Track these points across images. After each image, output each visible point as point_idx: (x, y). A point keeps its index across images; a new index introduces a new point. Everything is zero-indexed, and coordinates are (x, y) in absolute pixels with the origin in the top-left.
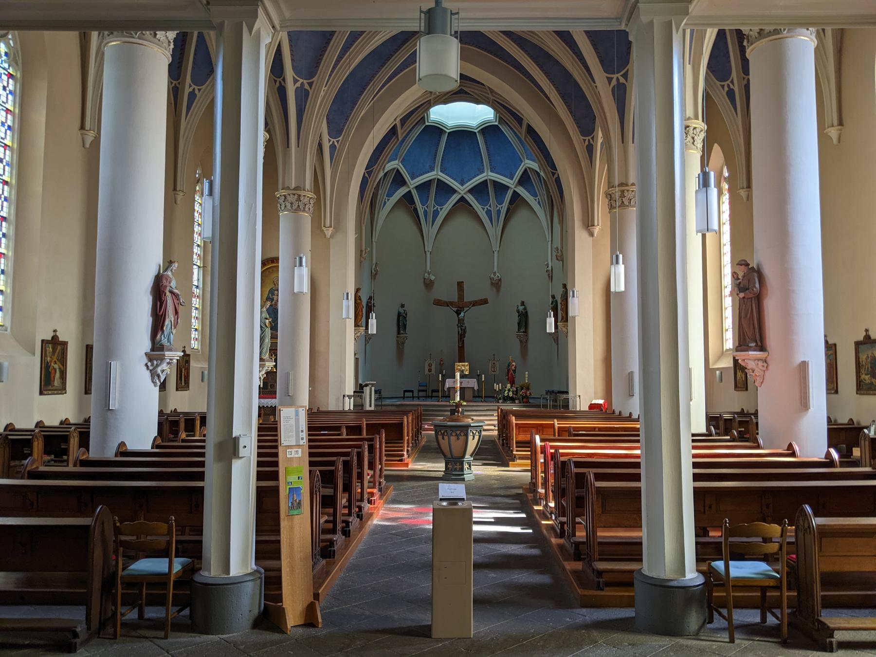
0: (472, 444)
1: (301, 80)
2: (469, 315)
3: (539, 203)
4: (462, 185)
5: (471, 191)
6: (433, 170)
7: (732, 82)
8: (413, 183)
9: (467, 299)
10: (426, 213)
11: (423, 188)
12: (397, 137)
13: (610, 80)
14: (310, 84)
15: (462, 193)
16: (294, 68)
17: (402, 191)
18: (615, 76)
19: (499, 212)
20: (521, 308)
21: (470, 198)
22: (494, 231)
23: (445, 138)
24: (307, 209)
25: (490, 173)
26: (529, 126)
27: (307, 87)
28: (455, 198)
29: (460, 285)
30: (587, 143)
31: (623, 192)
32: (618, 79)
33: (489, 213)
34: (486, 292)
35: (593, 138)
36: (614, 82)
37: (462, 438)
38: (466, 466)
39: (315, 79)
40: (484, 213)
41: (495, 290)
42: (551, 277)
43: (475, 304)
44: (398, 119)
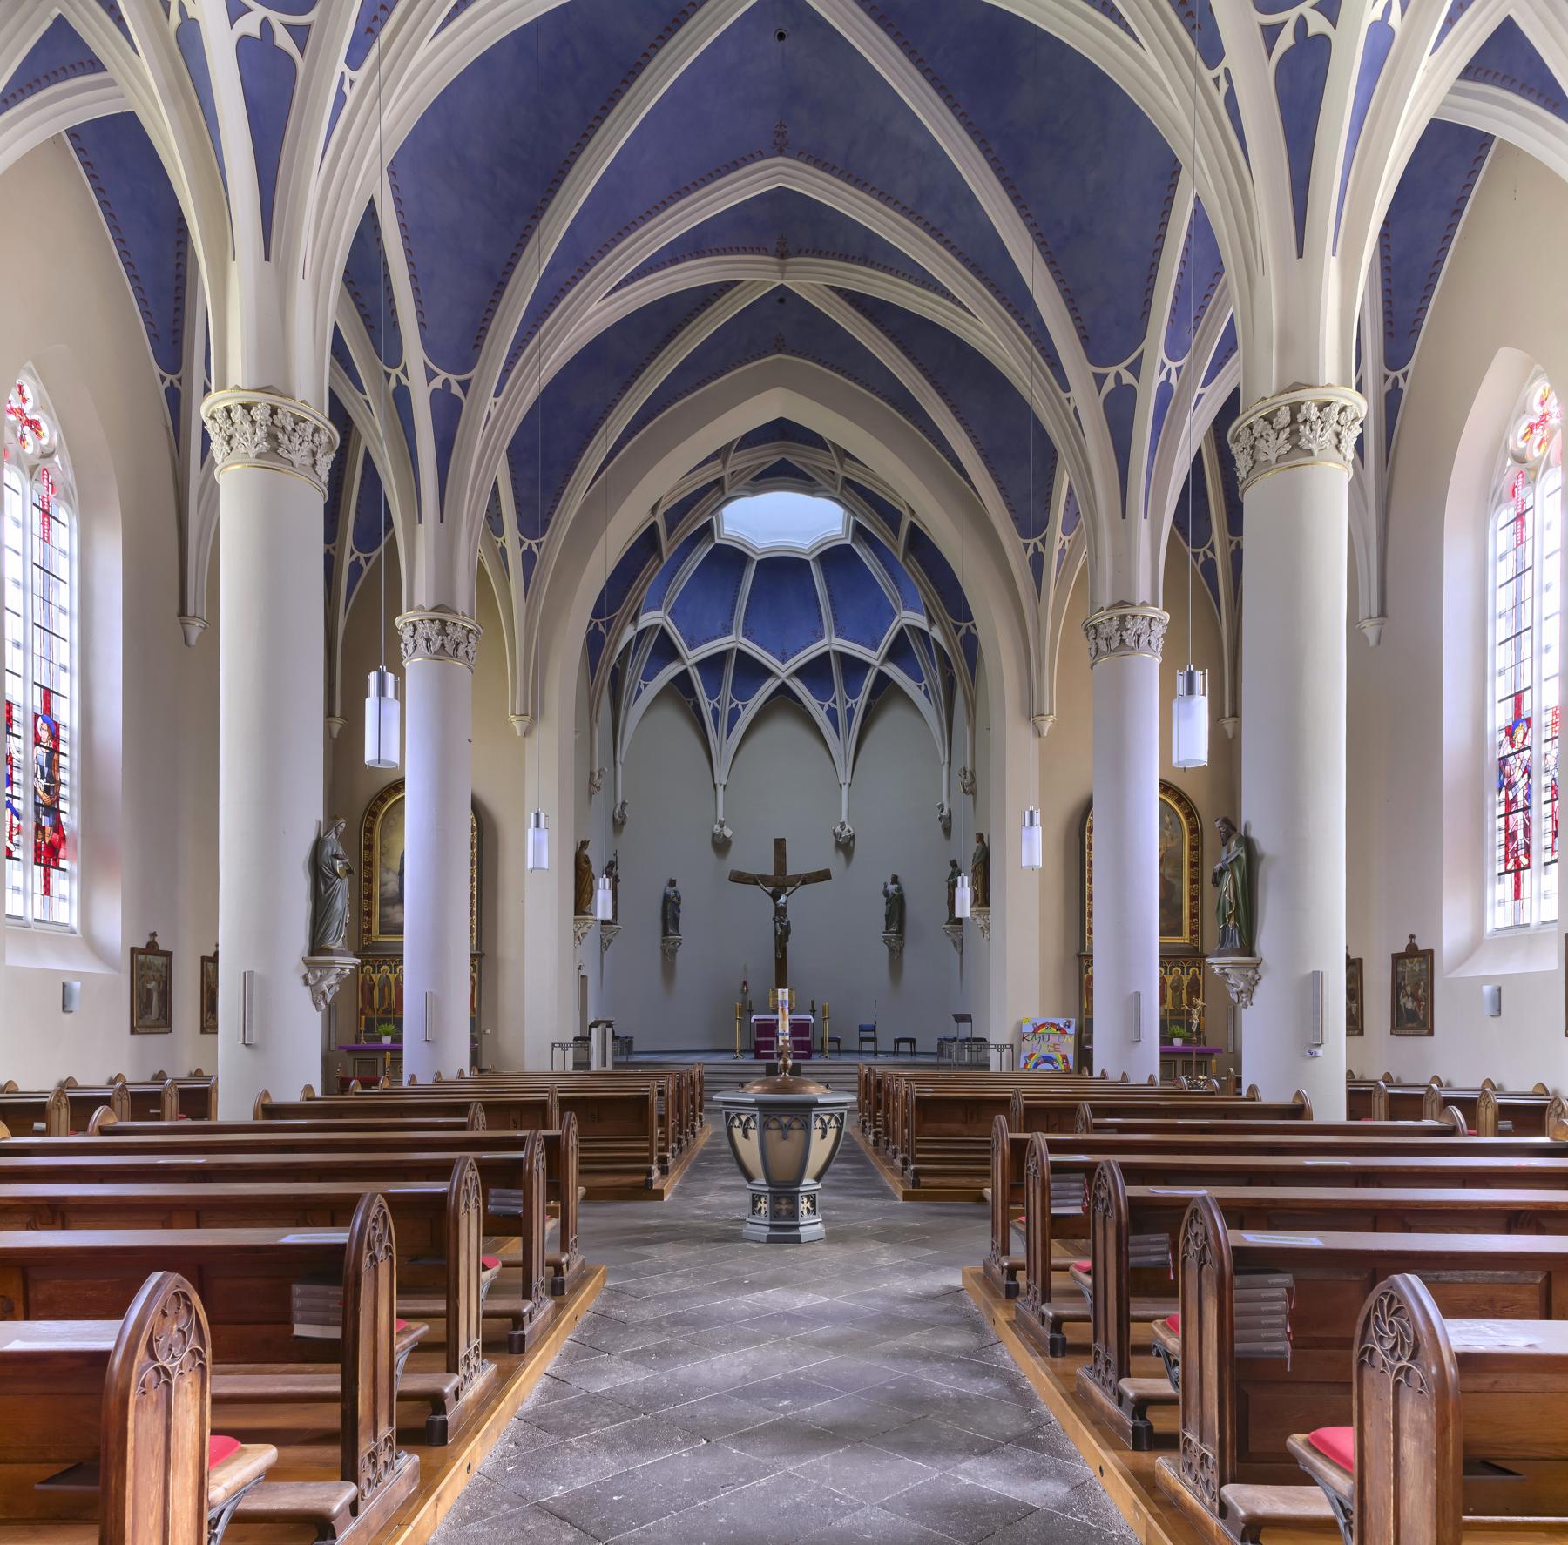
0: (820, 1149)
1: (443, 375)
2: (798, 901)
3: (926, 692)
4: (783, 662)
5: (799, 673)
6: (730, 633)
7: (1212, 549)
8: (692, 656)
9: (792, 869)
10: (715, 713)
11: (712, 666)
12: (660, 556)
13: (1100, 379)
14: (465, 385)
15: (783, 676)
16: (427, 345)
17: (672, 670)
18: (1112, 371)
19: (851, 712)
20: (892, 888)
21: (798, 687)
22: (842, 747)
23: (751, 572)
24: (461, 653)
25: (835, 640)
26: (914, 529)
27: (456, 390)
28: (769, 687)
29: (779, 844)
30: (1031, 551)
31: (1123, 618)
32: (1118, 376)
33: (832, 714)
34: (822, 856)
35: (1043, 541)
36: (963, 632)
37: (797, 1135)
38: (804, 1205)
39: (473, 373)
40: (823, 713)
41: (841, 854)
42: (947, 831)
43: (806, 879)
44: (660, 512)
